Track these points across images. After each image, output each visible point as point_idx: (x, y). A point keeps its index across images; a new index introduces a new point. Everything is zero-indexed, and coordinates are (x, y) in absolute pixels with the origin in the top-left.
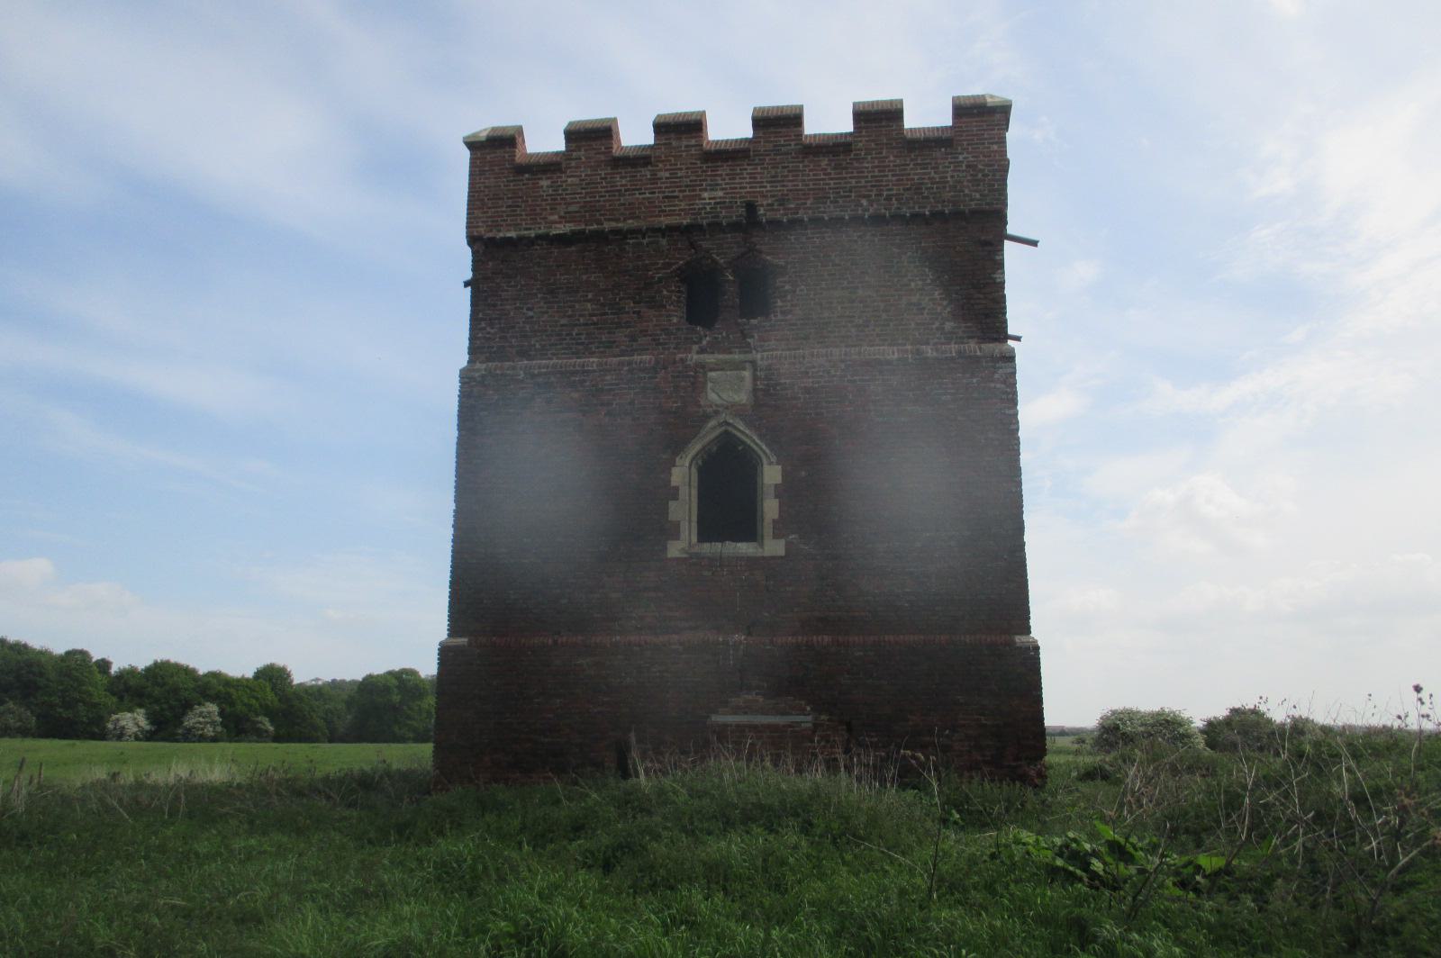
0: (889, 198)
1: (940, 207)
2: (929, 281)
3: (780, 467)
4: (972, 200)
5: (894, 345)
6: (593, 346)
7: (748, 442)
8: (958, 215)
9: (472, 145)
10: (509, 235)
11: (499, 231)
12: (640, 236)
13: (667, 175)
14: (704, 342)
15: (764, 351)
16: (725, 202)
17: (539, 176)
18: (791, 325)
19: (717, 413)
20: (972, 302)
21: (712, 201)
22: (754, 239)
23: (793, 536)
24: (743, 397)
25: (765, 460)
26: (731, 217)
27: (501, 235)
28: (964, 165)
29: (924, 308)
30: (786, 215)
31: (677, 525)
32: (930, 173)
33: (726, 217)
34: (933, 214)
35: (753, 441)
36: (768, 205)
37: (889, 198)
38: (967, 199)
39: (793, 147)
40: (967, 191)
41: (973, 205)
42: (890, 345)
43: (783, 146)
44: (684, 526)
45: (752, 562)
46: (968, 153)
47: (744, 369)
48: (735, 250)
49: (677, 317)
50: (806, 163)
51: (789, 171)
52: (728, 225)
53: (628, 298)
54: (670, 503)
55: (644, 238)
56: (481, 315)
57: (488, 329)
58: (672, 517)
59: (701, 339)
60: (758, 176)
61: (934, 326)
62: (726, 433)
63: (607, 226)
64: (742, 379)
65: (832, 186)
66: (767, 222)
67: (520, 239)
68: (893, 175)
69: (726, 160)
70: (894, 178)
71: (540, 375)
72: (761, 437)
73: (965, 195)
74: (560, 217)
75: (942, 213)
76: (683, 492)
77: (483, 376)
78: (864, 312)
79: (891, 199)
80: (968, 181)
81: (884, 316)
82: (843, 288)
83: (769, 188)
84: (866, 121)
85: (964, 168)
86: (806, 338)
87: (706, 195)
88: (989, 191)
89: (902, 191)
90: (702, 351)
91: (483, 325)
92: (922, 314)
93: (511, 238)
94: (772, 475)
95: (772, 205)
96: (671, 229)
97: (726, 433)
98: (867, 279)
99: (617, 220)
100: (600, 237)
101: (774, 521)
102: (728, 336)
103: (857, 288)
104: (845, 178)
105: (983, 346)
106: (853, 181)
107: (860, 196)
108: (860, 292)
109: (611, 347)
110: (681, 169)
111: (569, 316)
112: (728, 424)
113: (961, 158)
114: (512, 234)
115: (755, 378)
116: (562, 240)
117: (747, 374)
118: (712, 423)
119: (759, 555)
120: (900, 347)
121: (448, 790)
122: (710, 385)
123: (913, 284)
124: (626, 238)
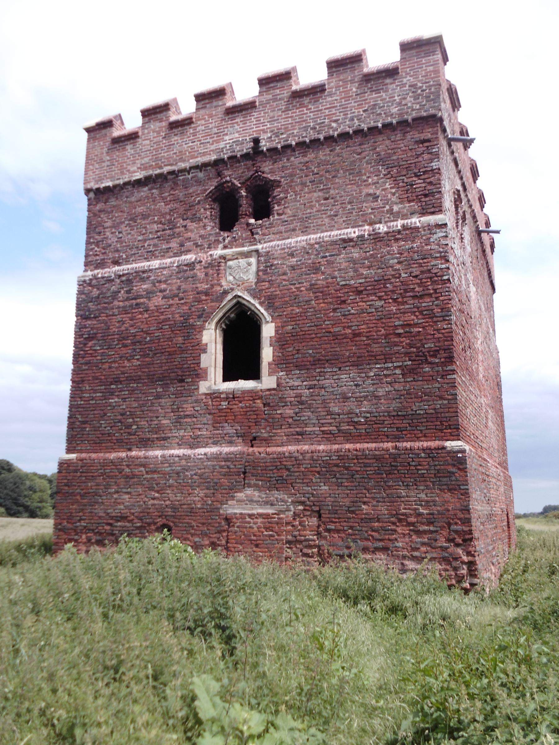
0: (352, 119)
1: (389, 119)
2: (382, 176)
3: (274, 324)
4: (413, 110)
5: (355, 227)
6: (157, 252)
7: (253, 308)
8: (403, 123)
9: (89, 130)
10: (107, 184)
11: (102, 183)
12: (186, 173)
13: (203, 128)
14: (227, 241)
15: (265, 242)
16: (239, 141)
17: (126, 143)
18: (283, 222)
19: (232, 289)
20: (435, 319)
21: (231, 141)
22: (259, 164)
23: (282, 373)
24: (251, 277)
25: (263, 321)
26: (243, 150)
27: (103, 185)
28: (407, 86)
29: (378, 197)
30: (280, 142)
31: (205, 371)
32: (382, 96)
33: (239, 151)
34: (384, 126)
35: (256, 307)
36: (268, 138)
37: (352, 119)
38: (409, 110)
39: (285, 95)
40: (409, 105)
41: (414, 114)
42: (353, 227)
43: (279, 95)
44: (211, 371)
45: (253, 395)
46: (410, 76)
47: (251, 257)
48: (246, 173)
49: (211, 227)
50: (294, 104)
51: (283, 112)
52: (241, 156)
53: (179, 217)
54: (202, 355)
55: (189, 174)
56: (92, 240)
57: (96, 249)
58: (203, 365)
59: (224, 240)
60: (262, 119)
61: (385, 209)
62: (238, 303)
63: (166, 169)
64: (249, 264)
65: (312, 117)
66: (267, 150)
67: (115, 186)
68: (355, 102)
69: (241, 111)
70: (356, 104)
71: (123, 275)
72: (261, 304)
73: (408, 108)
74: (138, 168)
75: (391, 124)
76: (211, 348)
77: (91, 280)
78: (335, 205)
79: (353, 120)
80: (410, 97)
81: (349, 207)
82: (320, 190)
83: (269, 126)
84: (336, 67)
85: (407, 88)
86: (294, 230)
87: (227, 138)
88: (427, 101)
89: (362, 113)
90: (225, 247)
91: (93, 246)
92: (377, 201)
93: (109, 186)
94: (268, 331)
95: (271, 137)
96: (205, 165)
97: (238, 303)
98: (337, 180)
99: (171, 165)
100: (162, 178)
101: (269, 364)
102: (242, 234)
103: (330, 188)
104: (322, 110)
105: (422, 219)
106: (327, 111)
107: (331, 121)
108: (332, 192)
109: (168, 252)
110: (212, 123)
111: (144, 234)
112: (240, 297)
113: (405, 80)
114: (110, 184)
115: (258, 262)
116: (139, 183)
117: (253, 260)
118: (229, 297)
119: (259, 388)
120: (360, 228)
121: (104, 545)
122: (228, 271)
123: (370, 180)
124: (177, 176)
